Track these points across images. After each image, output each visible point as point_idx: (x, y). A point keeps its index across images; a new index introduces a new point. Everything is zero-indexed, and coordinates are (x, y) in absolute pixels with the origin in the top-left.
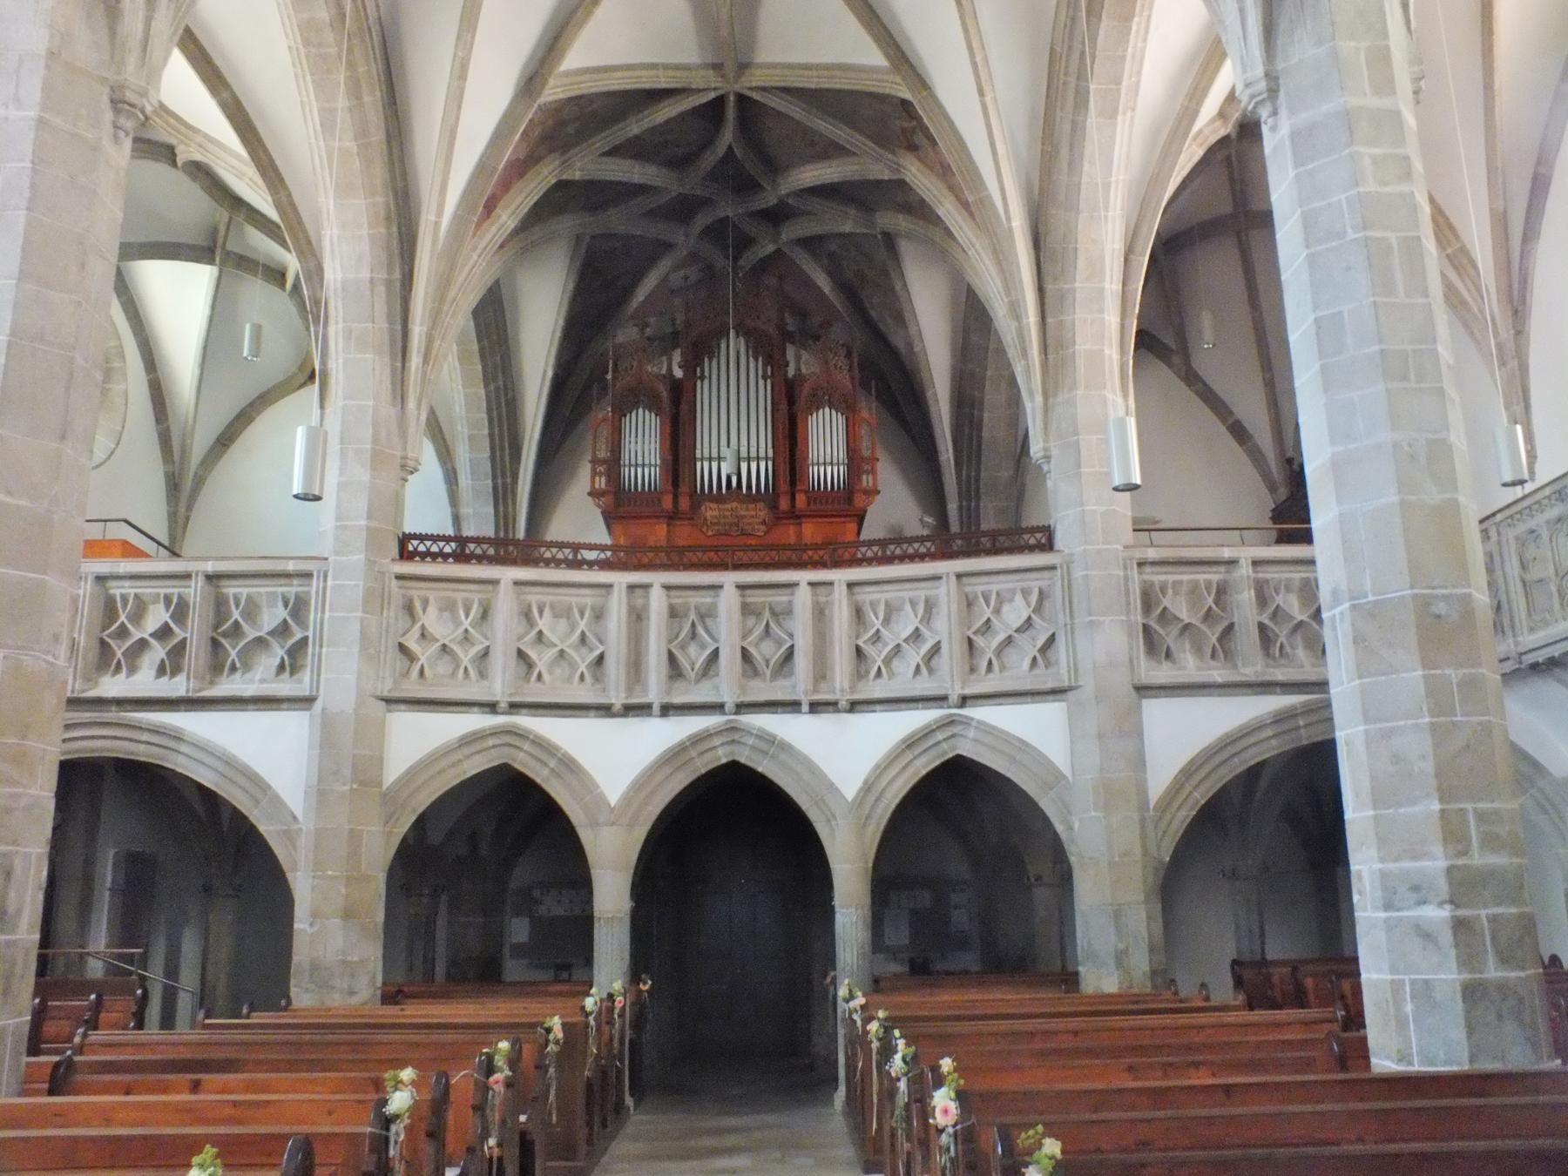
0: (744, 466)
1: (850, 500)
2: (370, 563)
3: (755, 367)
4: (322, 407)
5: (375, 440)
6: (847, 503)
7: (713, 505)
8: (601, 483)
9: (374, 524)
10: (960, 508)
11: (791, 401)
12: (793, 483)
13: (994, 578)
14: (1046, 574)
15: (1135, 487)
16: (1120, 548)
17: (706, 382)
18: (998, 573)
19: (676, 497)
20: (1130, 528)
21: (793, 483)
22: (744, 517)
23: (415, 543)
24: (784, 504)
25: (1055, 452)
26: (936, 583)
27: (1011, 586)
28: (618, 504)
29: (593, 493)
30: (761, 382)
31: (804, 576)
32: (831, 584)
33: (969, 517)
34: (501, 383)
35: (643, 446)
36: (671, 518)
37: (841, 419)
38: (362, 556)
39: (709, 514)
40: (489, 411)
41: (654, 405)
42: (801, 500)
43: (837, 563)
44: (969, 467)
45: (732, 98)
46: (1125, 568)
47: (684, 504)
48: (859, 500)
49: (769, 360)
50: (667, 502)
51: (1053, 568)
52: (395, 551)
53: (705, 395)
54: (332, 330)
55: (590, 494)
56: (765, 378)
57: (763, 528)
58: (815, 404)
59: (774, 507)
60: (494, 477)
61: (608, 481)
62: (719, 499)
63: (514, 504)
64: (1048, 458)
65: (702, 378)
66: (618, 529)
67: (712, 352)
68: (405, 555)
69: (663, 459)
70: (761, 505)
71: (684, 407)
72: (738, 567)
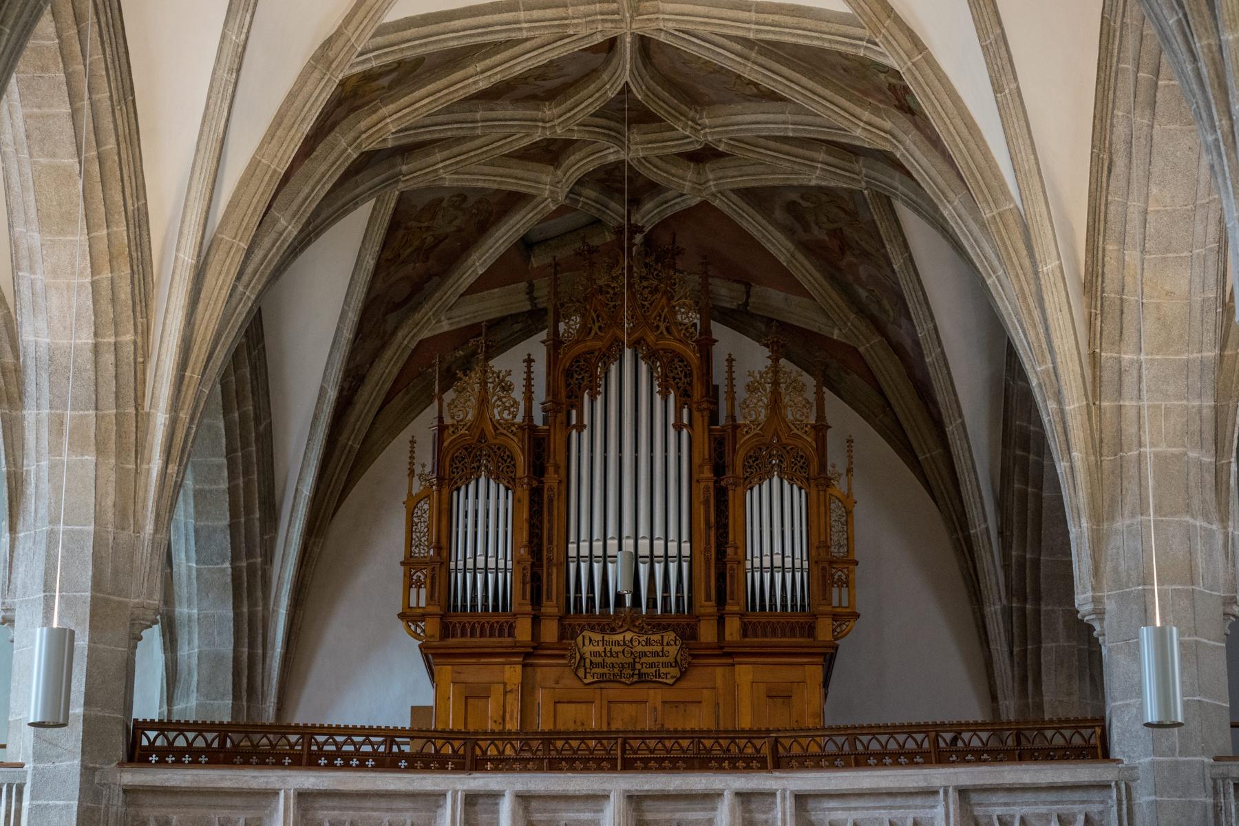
0: (643, 569)
1: (811, 630)
2: (87, 772)
3: (665, 409)
4: (13, 529)
5: (97, 583)
6: (805, 632)
7: (597, 637)
8: (420, 598)
9: (96, 711)
10: (1008, 613)
11: (719, 469)
12: (721, 600)
13: (1019, 797)
14: (1095, 795)
15: (1180, 725)
16: (1208, 760)
17: (586, 434)
18: (1025, 789)
19: (536, 621)
20: (1227, 727)
21: (721, 600)
22: (644, 654)
23: (152, 734)
24: (707, 633)
25: (1110, 606)
26: (930, 801)
27: (1043, 809)
28: (447, 630)
29: (408, 616)
30: (672, 433)
31: (730, 783)
32: (772, 794)
33: (1024, 627)
34: (250, 408)
35: (487, 526)
36: (527, 655)
37: (799, 498)
38: (77, 762)
39: (588, 649)
40: (230, 451)
41: (504, 473)
42: (733, 628)
43: (779, 762)
44: (1023, 546)
45: (628, 39)
46: (1216, 793)
47: (550, 632)
48: (824, 630)
49: (685, 396)
50: (523, 631)
51: (1105, 786)
52: (121, 753)
53: (585, 455)
54: (30, 414)
55: (402, 616)
56: (679, 427)
57: (675, 672)
58: (757, 471)
59: (688, 634)
60: (235, 559)
61: (431, 597)
62: (606, 626)
63: (266, 597)
64: (1100, 613)
65: (580, 427)
66: (446, 671)
67: (594, 385)
68: (136, 755)
69: (518, 561)
70: (670, 636)
71: (551, 479)
72: (628, 765)
